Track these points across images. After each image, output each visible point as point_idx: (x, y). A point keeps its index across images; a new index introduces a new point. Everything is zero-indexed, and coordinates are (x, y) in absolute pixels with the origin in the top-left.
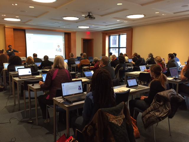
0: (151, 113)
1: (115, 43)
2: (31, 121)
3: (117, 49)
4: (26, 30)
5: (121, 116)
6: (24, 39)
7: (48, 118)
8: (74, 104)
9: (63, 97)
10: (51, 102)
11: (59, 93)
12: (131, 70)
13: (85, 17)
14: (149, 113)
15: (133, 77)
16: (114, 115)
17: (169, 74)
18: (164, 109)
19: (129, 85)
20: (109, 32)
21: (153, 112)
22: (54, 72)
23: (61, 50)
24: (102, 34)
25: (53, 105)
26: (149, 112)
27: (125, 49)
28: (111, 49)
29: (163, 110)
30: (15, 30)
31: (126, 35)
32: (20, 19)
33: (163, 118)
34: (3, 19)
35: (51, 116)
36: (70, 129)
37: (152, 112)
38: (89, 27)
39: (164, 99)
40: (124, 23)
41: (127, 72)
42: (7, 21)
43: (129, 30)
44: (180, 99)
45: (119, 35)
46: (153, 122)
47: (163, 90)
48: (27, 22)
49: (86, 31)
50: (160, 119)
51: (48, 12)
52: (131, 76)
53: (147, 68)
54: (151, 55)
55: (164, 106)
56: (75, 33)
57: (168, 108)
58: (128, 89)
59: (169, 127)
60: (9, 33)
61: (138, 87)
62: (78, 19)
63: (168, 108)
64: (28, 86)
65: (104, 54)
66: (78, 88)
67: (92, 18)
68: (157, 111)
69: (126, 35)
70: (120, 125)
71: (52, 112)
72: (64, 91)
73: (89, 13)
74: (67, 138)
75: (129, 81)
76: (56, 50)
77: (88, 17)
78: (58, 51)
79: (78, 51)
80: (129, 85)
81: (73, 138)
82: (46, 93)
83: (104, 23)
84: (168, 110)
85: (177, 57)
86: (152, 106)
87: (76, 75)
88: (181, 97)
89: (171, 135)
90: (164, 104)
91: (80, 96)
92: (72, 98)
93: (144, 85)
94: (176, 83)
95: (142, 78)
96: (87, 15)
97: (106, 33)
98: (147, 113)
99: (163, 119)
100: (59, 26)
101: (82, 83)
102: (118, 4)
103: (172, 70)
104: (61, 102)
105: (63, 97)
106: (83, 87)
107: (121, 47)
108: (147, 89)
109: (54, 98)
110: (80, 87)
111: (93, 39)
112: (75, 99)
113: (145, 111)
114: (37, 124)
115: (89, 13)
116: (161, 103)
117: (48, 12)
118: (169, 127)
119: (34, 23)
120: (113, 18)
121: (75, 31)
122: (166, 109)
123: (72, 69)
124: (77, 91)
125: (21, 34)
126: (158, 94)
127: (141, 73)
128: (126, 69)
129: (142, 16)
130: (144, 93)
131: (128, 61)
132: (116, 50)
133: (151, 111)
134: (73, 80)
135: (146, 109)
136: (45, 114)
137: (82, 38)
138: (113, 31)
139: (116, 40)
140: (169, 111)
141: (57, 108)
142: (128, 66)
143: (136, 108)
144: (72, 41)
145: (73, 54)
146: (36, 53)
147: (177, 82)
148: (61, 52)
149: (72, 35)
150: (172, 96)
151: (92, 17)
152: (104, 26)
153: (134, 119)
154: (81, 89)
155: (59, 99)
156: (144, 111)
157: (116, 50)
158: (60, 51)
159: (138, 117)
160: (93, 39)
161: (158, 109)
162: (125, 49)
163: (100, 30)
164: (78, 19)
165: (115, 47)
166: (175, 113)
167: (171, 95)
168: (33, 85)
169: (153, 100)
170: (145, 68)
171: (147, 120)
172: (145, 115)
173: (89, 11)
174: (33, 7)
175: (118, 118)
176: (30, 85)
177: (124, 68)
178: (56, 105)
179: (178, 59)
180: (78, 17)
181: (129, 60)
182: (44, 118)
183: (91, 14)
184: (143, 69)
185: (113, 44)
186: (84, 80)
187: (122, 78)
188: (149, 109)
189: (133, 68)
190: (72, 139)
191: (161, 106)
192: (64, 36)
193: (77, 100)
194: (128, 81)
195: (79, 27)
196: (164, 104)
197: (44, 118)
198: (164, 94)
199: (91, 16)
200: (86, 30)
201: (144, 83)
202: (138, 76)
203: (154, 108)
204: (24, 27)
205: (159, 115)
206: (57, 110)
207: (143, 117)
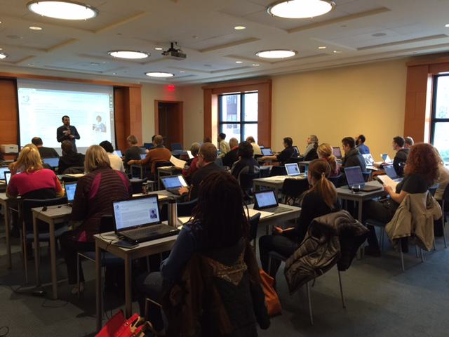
0: (301, 259)
1: (232, 111)
2: (41, 292)
3: (239, 125)
4: (18, 80)
5: (239, 265)
6: (14, 101)
7: (80, 281)
8: (142, 245)
9: (118, 232)
10: (90, 245)
11: (109, 224)
12: (266, 173)
13: (163, 54)
14: (297, 260)
15: (269, 188)
16: (225, 264)
17: (341, 182)
18: (327, 252)
19: (260, 205)
20: (217, 87)
21: (306, 258)
22: (92, 181)
23: (105, 128)
25: (95, 251)
26: (299, 257)
27: (256, 125)
28: (224, 126)
29: (325, 253)
31: (257, 94)
33: (326, 269)
35: (87, 278)
36: (133, 303)
37: (304, 258)
39: (327, 231)
41: (258, 178)
42: (160, 78)
43: (264, 84)
44: (358, 230)
45: (242, 95)
46: (306, 278)
47: (327, 211)
48: (22, 60)
49: (163, 83)
50: (319, 271)
52: (267, 185)
53: (302, 170)
54: (315, 140)
55: (327, 244)
56: (139, 87)
57: (334, 249)
58: (257, 212)
59: (341, 291)
61: (278, 209)
62: (146, 56)
63: (334, 249)
64: (31, 212)
65: (208, 139)
66: (149, 214)
68: (314, 256)
70: (236, 284)
71: (91, 271)
72: (119, 219)
73: (172, 44)
74: (127, 318)
75: (261, 197)
76: (94, 127)
77: (170, 53)
78: (98, 130)
79: (147, 129)
80: (260, 205)
81: (139, 317)
82: (73, 227)
83: (206, 66)
84: (334, 251)
86: (303, 247)
87: (144, 185)
88: (360, 226)
89: (344, 307)
90: (327, 241)
91: (154, 229)
92: (136, 233)
93: (294, 205)
94: (355, 200)
95: (289, 190)
96: (167, 49)
97: (213, 89)
98: (295, 261)
99: (324, 272)
100: (101, 72)
101: (159, 202)
102: (236, 28)
103: (350, 172)
104: (113, 242)
105: (118, 232)
106: (161, 207)
107: (246, 120)
108: (294, 212)
109: (97, 236)
110: (153, 212)
111: (182, 102)
112: (144, 235)
113: (292, 256)
114: (55, 296)
115: (172, 44)
116: (322, 240)
118: (341, 291)
119: (40, 63)
121: (139, 83)
122: (331, 250)
123: (134, 174)
124: (148, 219)
126: (315, 221)
127: (286, 180)
128: (255, 172)
129: (290, 54)
130: (288, 220)
132: (236, 127)
133: (302, 257)
134: (134, 196)
135: (292, 253)
136: (75, 274)
137: (155, 101)
138: (239, 84)
139: (236, 105)
140: (337, 254)
141: (102, 258)
142: (261, 164)
143: (273, 253)
144: (131, 106)
145: (137, 138)
146: (38, 136)
147: (360, 197)
148: (105, 131)
149: (132, 92)
150: (342, 224)
153: (271, 275)
154: (156, 217)
155: (108, 238)
156: (288, 257)
157: (236, 127)
158: (103, 129)
159: (277, 273)
160: (182, 102)
161: (315, 251)
162: (256, 125)
163: (198, 82)
164: (146, 56)
165: (233, 121)
166: (351, 260)
167: (341, 223)
168: (45, 210)
169: (305, 233)
170: (296, 169)
171: (293, 276)
172: (291, 265)
174: (40, 29)
175: (233, 269)
176: (39, 210)
177: (252, 168)
178: (102, 251)
179: (367, 148)
180: (145, 53)
181: (264, 150)
182: (73, 281)
183: (175, 47)
184: (293, 171)
185: (228, 114)
186: (162, 196)
187: (246, 192)
188: (299, 252)
189: (271, 169)
190: (137, 319)
191: (321, 244)
192: (112, 96)
193: (147, 238)
194: (257, 195)
196: (327, 241)
197: (73, 281)
198: (327, 221)
199: (177, 51)
201: (294, 200)
202: (281, 187)
203: (307, 249)
204: (12, 72)
205: (318, 263)
206: (103, 263)
207: (286, 269)
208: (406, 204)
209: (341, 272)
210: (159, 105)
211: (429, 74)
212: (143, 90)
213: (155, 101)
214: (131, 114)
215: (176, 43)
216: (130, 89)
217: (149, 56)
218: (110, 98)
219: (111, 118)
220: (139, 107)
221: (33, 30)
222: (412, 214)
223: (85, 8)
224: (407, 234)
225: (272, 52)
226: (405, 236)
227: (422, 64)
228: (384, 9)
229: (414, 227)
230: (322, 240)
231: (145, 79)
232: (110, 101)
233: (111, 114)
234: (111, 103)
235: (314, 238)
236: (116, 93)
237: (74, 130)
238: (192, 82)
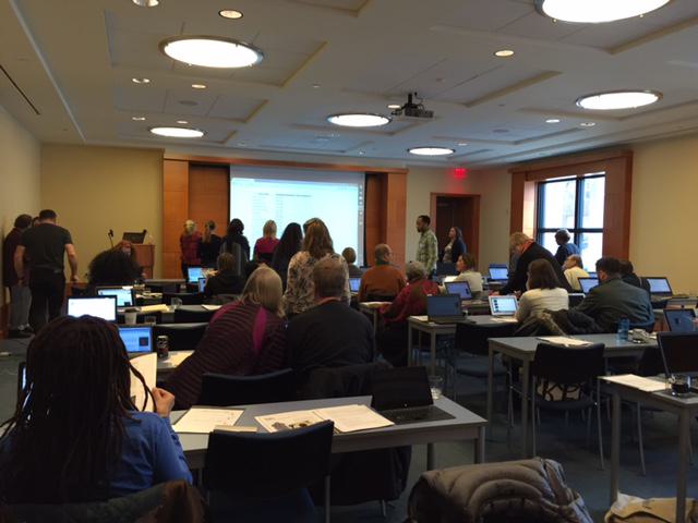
6: (225, 198)
24: (510, 176)
27: (600, 235)
30: (195, 165)
31: (603, 179)
32: (201, 131)
34: (408, 150)
42: (162, 137)
45: (579, 181)
51: (266, 101)
56: (403, 173)
60: (177, 174)
69: (603, 179)
73: (410, 96)
100: (343, 152)
107: (585, 225)
111: (479, 196)
114: (567, 414)
115: (410, 96)
117: (266, 101)
121: (404, 167)
125: (210, 179)
129: (647, 99)
131: (578, 288)
137: (432, 194)
138: (572, 161)
149: (392, 182)
152: (507, 146)
162: (600, 235)
163: (500, 161)
164: (384, 121)
173: (413, 89)
192: (362, 187)
198: (450, 490)
199: (416, 107)
200: (443, 162)
209: (207, 436)
210: (438, 202)
211: (526, 184)
212: (410, 178)
213: (432, 194)
217: (390, 121)
218: (360, 190)
219: (359, 221)
223: (233, 45)
225: (603, 97)
231: (409, 160)
237: (419, 231)
238: (488, 163)
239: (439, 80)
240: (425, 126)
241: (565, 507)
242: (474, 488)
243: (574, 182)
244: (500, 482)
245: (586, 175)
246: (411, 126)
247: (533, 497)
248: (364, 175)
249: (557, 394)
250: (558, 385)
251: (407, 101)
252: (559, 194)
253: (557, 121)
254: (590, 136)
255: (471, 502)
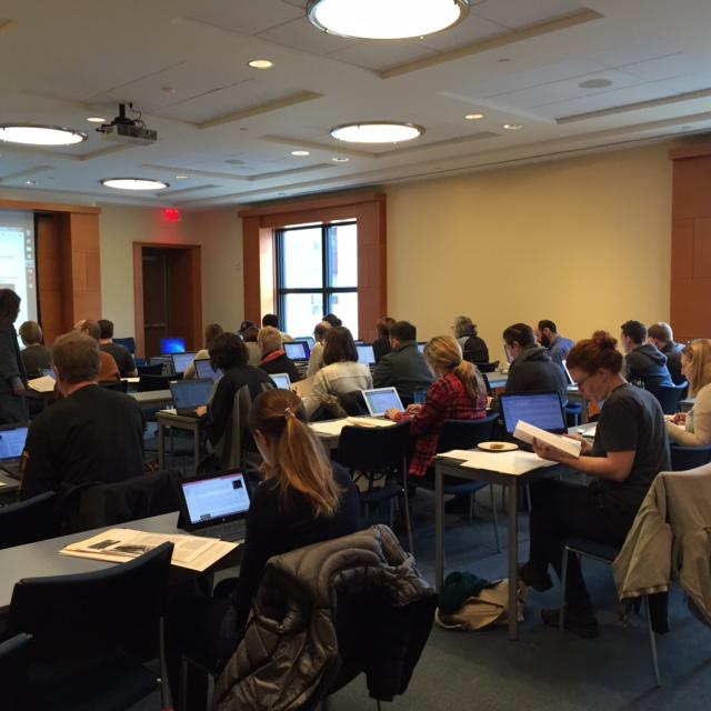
3: (319, 297)
24: (240, 220)
27: (355, 295)
31: (355, 226)
34: (102, 182)
38: (163, 186)
40: (332, 165)
44: (401, 587)
56: (92, 213)
67: (135, 133)
69: (355, 226)
73: (122, 108)
77: (115, 127)
80: (195, 516)
85: (563, 336)
90: (305, 624)
97: (262, 217)
111: (199, 247)
115: (122, 108)
116: (288, 622)
120: (188, 122)
121: (94, 205)
122: (313, 654)
127: (346, 429)
129: (407, 134)
137: (135, 243)
138: (317, 204)
140: (330, 662)
149: (77, 228)
150: (346, 573)
151: (140, 129)
161: (268, 659)
162: (355, 295)
164: (77, 139)
173: (126, 97)
183: (129, 115)
192: (30, 232)
195: (109, 184)
198: (298, 567)
199: (132, 123)
201: (371, 480)
208: (656, 500)
211: (261, 230)
214: (75, 276)
215: (131, 105)
216: (72, 216)
217: (85, 139)
218: (26, 237)
219: (28, 282)
220: (94, 258)
221: (479, 114)
222: (673, 530)
224: (657, 586)
226: (652, 591)
227: (703, 153)
228: (586, 15)
229: (677, 563)
230: (288, 622)
232: (26, 245)
233: (28, 275)
234: (29, 249)
235: (263, 619)
236: (42, 226)
239: (167, 89)
240: (137, 151)
241: (400, 567)
242: (320, 566)
243: (320, 230)
244: (356, 550)
245: (333, 222)
246: (114, 148)
247: (373, 562)
248: (32, 216)
249: (363, 484)
250: (364, 474)
251: (118, 115)
252: (302, 243)
253: (306, 153)
254: (339, 174)
255: (321, 578)
